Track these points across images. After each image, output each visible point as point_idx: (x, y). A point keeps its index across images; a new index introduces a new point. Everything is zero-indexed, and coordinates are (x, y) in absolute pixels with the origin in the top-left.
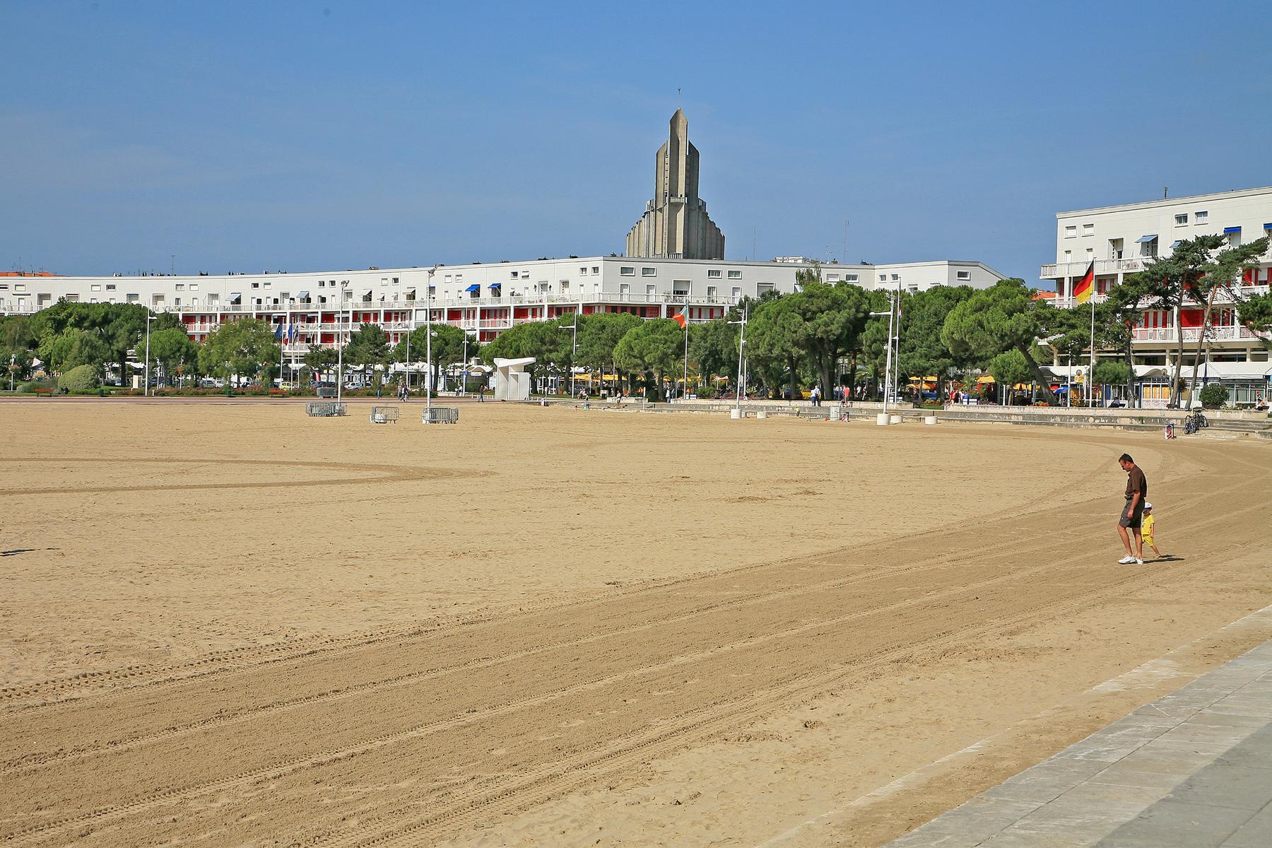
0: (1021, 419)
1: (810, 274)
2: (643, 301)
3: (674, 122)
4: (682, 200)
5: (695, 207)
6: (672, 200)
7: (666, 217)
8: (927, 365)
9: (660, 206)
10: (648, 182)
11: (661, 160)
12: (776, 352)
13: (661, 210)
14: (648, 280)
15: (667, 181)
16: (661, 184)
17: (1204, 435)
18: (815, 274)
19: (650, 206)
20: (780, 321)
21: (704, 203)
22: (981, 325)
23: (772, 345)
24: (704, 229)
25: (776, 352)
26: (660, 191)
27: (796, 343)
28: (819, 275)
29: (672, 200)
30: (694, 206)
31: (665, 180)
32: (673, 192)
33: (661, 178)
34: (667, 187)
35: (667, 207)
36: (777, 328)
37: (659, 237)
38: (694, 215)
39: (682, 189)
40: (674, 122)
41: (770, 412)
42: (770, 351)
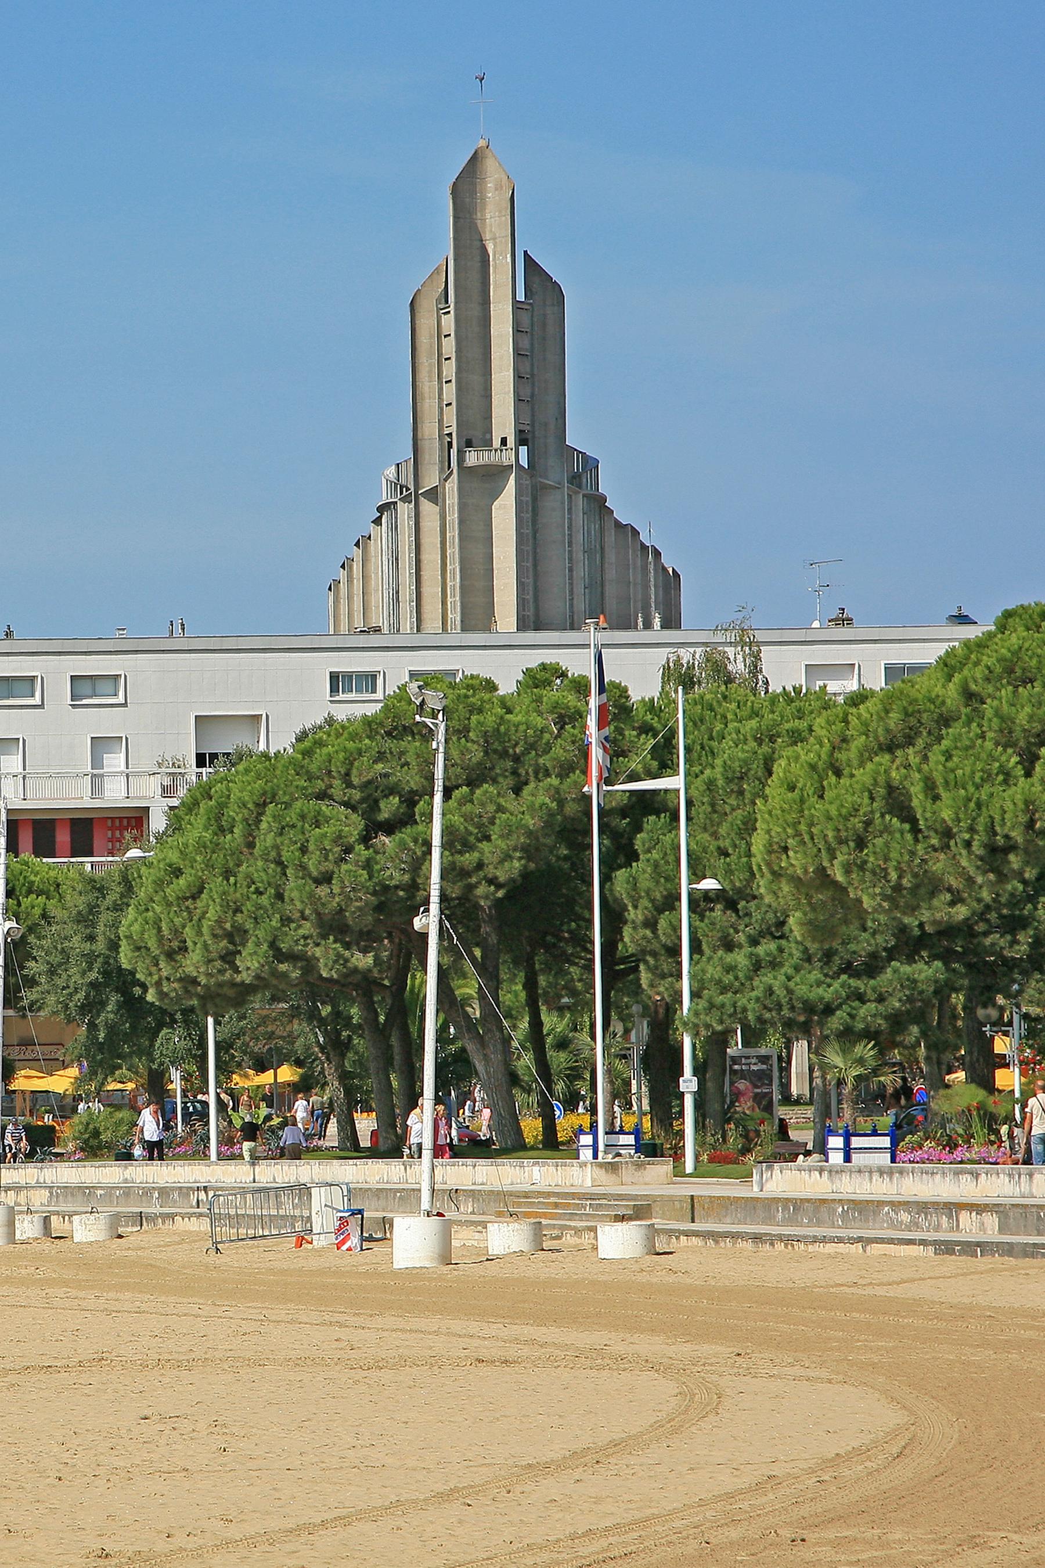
0: (989, 1229)
1: (718, 668)
2: (73, 795)
3: (466, 189)
4: (507, 458)
5: (558, 477)
6: (472, 458)
7: (453, 517)
8: (827, 993)
9: (431, 479)
10: (376, 403)
11: (427, 323)
12: (250, 963)
13: (433, 495)
14: (102, 721)
15: (450, 392)
16: (429, 406)
17: (806, 1553)
18: (738, 666)
19: (398, 486)
20: (266, 838)
21: (591, 465)
22: (897, 803)
23: (236, 936)
24: (597, 552)
25: (250, 963)
26: (430, 430)
27: (334, 926)
28: (755, 669)
29: (472, 458)
30: (555, 473)
31: (441, 399)
32: (474, 432)
33: (428, 385)
34: (451, 417)
35: (452, 486)
36: (256, 868)
37: (431, 590)
38: (553, 505)
39: (504, 420)
40: (466, 189)
41: (132, 1216)
42: (229, 958)
